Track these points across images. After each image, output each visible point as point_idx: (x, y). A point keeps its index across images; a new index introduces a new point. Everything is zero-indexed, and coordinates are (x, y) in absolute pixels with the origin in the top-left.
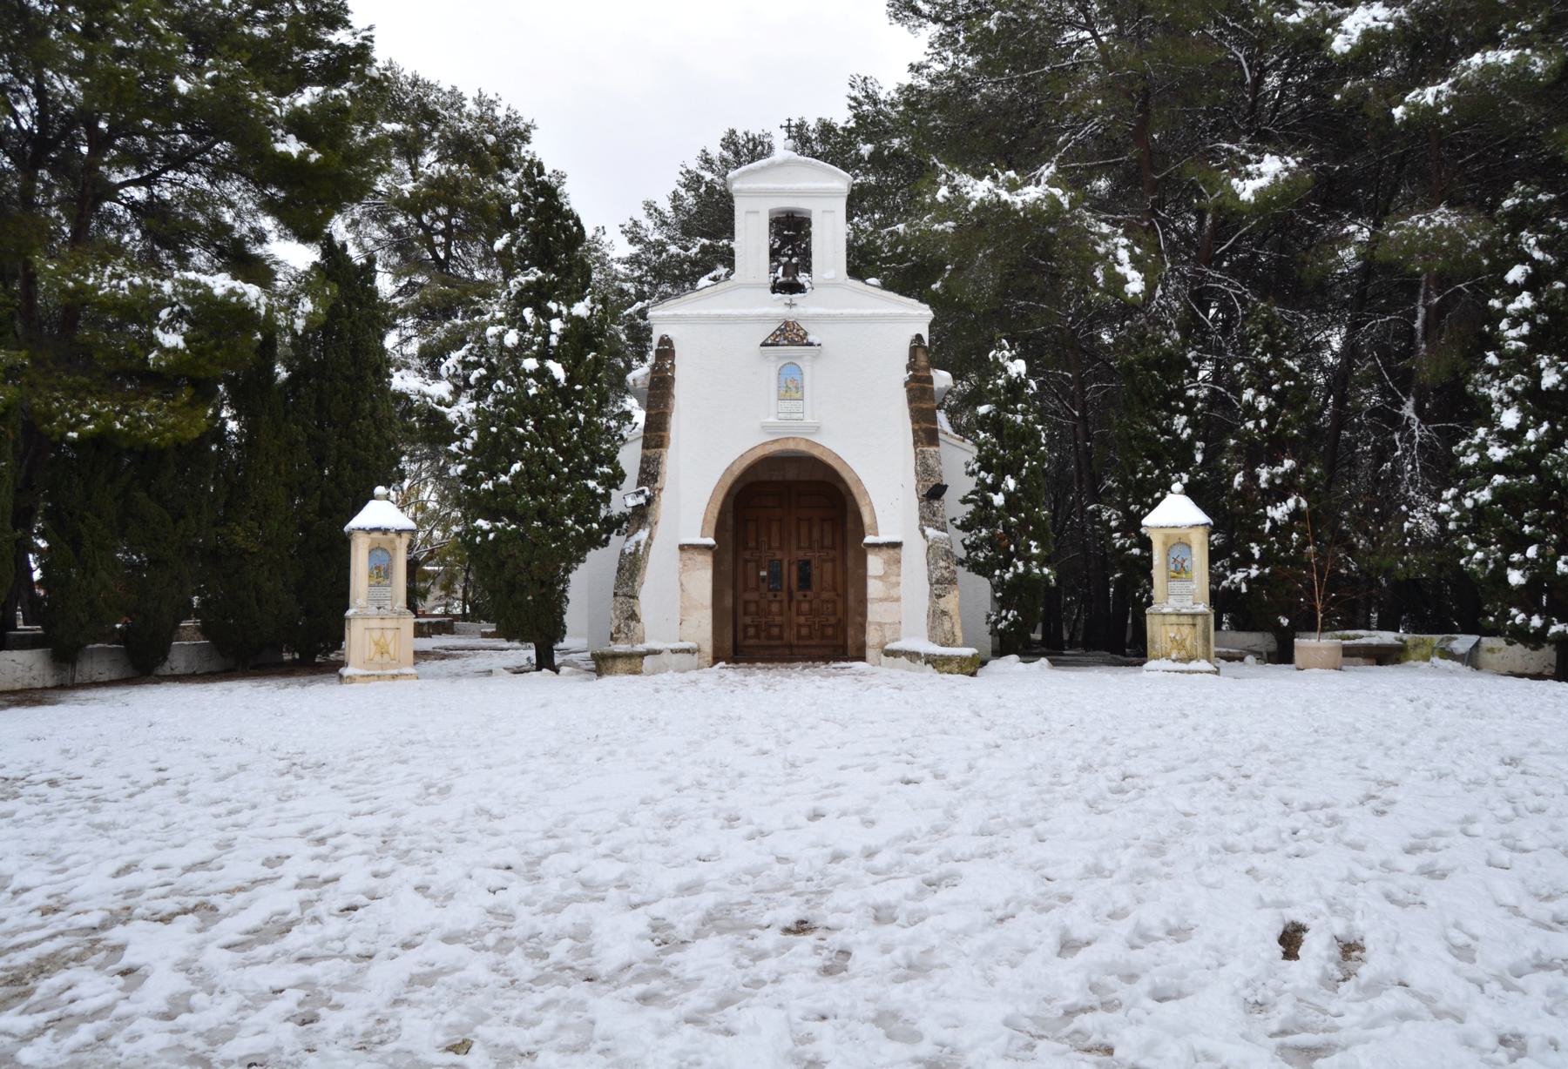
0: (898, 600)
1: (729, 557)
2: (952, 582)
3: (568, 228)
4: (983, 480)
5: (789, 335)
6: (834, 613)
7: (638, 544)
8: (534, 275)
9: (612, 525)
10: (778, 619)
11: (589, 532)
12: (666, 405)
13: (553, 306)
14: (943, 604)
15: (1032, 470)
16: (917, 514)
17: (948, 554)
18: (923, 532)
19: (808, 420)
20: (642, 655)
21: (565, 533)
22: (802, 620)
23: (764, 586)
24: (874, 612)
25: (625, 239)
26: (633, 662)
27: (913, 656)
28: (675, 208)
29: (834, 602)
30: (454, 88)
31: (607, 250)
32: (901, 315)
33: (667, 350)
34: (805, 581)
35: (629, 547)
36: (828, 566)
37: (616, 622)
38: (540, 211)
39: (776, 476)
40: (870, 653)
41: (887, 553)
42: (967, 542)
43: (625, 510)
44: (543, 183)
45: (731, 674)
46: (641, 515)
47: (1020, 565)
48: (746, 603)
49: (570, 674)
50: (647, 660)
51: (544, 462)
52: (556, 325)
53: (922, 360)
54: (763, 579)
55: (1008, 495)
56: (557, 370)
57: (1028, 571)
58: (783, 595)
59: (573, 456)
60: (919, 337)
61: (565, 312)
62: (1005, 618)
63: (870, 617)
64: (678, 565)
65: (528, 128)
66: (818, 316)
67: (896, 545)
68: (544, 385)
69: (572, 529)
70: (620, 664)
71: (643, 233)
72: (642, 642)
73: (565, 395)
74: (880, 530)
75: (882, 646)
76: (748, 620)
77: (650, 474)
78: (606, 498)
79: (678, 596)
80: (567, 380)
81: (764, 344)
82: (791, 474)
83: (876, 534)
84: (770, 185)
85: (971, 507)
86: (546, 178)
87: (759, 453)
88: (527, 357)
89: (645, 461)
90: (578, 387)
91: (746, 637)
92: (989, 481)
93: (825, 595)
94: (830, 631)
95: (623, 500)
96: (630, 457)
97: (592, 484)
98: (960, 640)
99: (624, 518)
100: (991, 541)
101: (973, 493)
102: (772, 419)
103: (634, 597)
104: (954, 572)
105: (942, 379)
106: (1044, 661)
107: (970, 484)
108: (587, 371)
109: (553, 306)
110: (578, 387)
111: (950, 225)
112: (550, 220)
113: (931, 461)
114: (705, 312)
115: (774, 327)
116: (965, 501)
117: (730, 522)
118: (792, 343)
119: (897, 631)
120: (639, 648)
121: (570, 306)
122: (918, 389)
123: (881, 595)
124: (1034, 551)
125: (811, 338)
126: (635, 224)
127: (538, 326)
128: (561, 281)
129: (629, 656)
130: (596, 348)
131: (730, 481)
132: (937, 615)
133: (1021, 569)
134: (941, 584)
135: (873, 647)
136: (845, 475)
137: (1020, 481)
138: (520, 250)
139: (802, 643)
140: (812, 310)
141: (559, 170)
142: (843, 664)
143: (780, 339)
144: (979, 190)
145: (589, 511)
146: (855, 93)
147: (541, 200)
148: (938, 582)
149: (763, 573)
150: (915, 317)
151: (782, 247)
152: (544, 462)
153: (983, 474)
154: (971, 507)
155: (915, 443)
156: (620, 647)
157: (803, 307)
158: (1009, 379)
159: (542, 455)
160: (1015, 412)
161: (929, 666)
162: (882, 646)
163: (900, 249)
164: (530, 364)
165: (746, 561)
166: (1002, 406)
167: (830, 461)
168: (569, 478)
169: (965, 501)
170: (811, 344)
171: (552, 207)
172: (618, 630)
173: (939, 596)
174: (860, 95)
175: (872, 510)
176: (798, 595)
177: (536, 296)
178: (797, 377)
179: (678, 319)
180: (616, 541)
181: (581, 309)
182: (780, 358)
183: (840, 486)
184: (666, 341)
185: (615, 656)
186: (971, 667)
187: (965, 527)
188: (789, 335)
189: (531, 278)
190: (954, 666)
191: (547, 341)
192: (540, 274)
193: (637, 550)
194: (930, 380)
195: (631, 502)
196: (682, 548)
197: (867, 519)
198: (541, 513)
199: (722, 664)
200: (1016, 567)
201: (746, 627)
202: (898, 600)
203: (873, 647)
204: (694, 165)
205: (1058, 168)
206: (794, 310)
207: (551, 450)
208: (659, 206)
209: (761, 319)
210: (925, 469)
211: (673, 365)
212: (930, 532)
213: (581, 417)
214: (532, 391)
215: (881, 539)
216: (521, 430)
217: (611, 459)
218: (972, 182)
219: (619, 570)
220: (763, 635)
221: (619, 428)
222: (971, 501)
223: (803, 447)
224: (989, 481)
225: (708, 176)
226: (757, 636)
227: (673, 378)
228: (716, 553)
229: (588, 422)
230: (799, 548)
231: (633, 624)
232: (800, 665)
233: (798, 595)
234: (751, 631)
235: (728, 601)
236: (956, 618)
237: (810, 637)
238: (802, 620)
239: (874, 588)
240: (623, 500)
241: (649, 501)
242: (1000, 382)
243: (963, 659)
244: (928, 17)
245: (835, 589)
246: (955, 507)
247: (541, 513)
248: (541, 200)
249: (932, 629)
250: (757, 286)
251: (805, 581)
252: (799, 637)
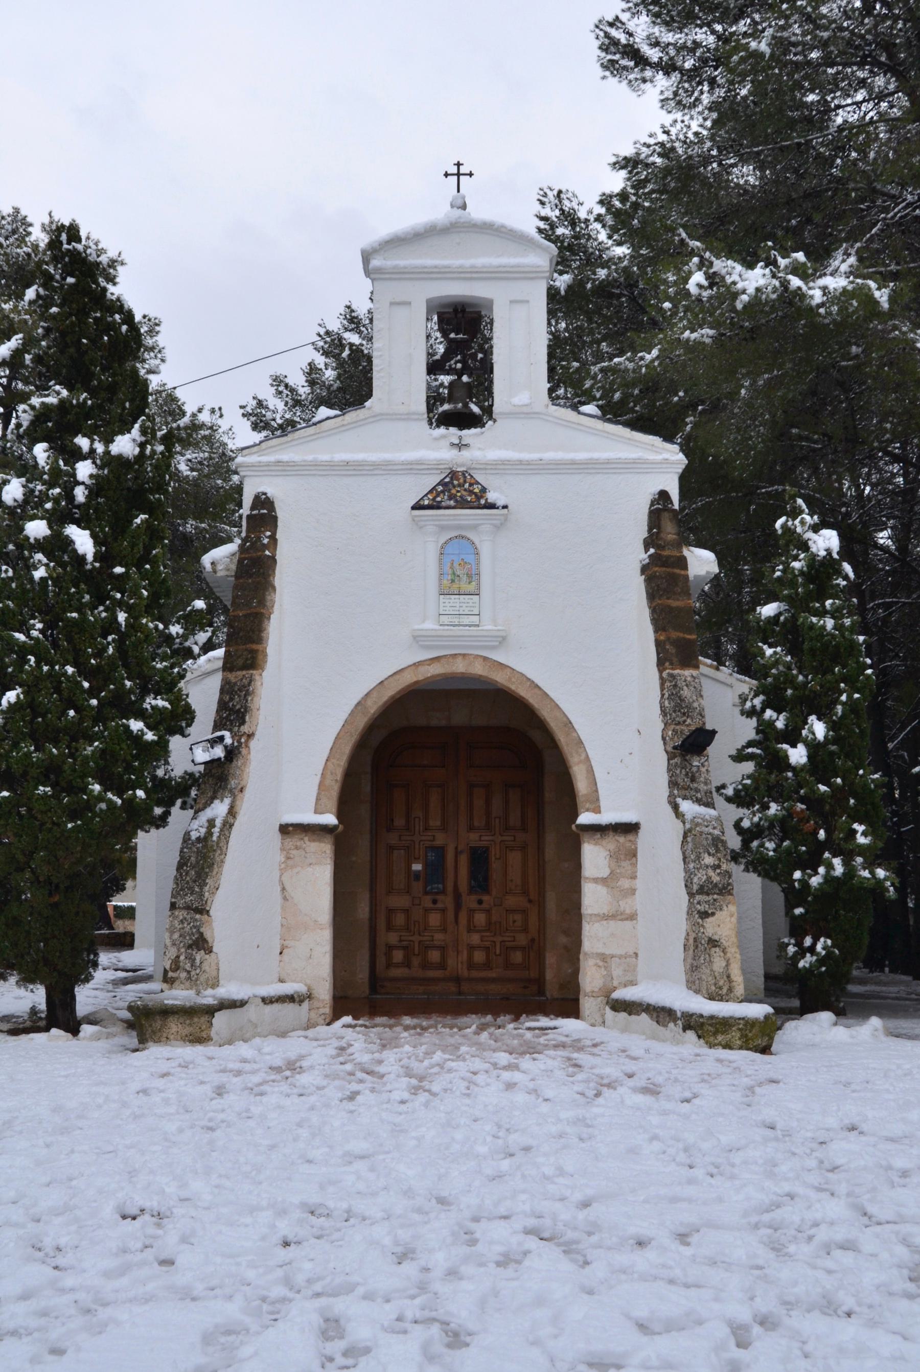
0: (632, 917)
1: (364, 843)
2: (725, 890)
3: (114, 327)
4: (771, 723)
5: (457, 492)
6: (525, 930)
7: (211, 823)
8: (57, 394)
9: (172, 792)
10: (439, 937)
11: (130, 803)
12: (262, 602)
13: (83, 442)
14: (711, 927)
15: (851, 706)
16: (663, 779)
17: (718, 843)
18: (676, 807)
19: (488, 626)
20: (210, 1011)
21: (89, 806)
22: (475, 939)
23: (417, 887)
24: (595, 937)
25: (247, 424)
26: (196, 1022)
27: (662, 1014)
28: (312, 383)
29: (524, 912)
30: (17, 211)
31: (225, 439)
32: (635, 462)
33: (265, 514)
34: (480, 877)
35: (198, 828)
36: (515, 858)
37: (173, 952)
38: (69, 297)
39: (437, 720)
40: (588, 1005)
41: (612, 842)
42: (746, 824)
43: (191, 768)
44: (74, 254)
45: (355, 1037)
46: (218, 777)
47: (837, 862)
48: (390, 911)
49: (96, 1037)
50: (220, 1019)
51: (58, 690)
52: (84, 470)
53: (670, 531)
54: (417, 875)
55: (814, 748)
56: (82, 541)
57: (850, 872)
58: (447, 901)
59: (108, 680)
60: (663, 495)
61: (100, 448)
62: (812, 950)
63: (588, 945)
64: (279, 857)
65: (113, 263)
66: (504, 462)
67: (631, 829)
68: (61, 564)
69: (101, 798)
70: (174, 1026)
71: (269, 415)
72: (215, 984)
73: (94, 581)
74: (603, 803)
75: (606, 993)
76: (393, 938)
77: (234, 711)
78: (160, 750)
79: (274, 907)
80: (97, 557)
81: (417, 507)
82: (460, 717)
83: (597, 810)
84: (429, 262)
85: (749, 767)
86: (80, 247)
87: (409, 679)
88: (33, 518)
89: (227, 689)
90: (119, 570)
91: (389, 965)
92: (780, 725)
93: (511, 901)
94: (518, 957)
95: (187, 754)
96: (202, 686)
97: (136, 725)
98: (740, 990)
99: (190, 780)
100: (784, 827)
101: (750, 744)
102: (430, 625)
103: (202, 910)
104: (728, 874)
105: (702, 562)
106: (875, 1022)
107: (748, 729)
108: (133, 546)
109: (83, 442)
110: (119, 570)
111: (706, 333)
112: (83, 313)
113: (686, 692)
114: (325, 457)
115: (432, 480)
116: (740, 757)
117: (366, 788)
118: (462, 504)
119: (633, 969)
120: (208, 997)
121: (108, 440)
122: (662, 575)
123: (605, 910)
124: (861, 840)
125: (491, 496)
126: (260, 404)
127: (55, 472)
128: (100, 407)
129: (189, 1012)
130: (150, 509)
131: (361, 722)
132: (701, 947)
133: (839, 868)
134: (706, 895)
135: (593, 995)
136: (546, 713)
137: (832, 726)
138: (38, 360)
139: (475, 974)
140: (494, 454)
141: (152, 315)
142: (544, 1022)
143: (443, 499)
144: (752, 280)
145: (129, 769)
146: (546, 211)
147: (70, 280)
148: (702, 890)
149: (417, 867)
150: (660, 464)
151: (447, 356)
152: (58, 690)
153: (769, 714)
154: (749, 767)
155: (661, 664)
156: (179, 996)
157: (482, 448)
158: (812, 559)
159: (56, 679)
160: (822, 613)
161: (691, 1035)
162: (606, 993)
163: (617, 395)
164: (37, 529)
165: (391, 848)
166: (798, 604)
167: (523, 692)
168: (100, 716)
169: (740, 757)
170: (492, 506)
171: (89, 292)
172: (176, 965)
173: (705, 915)
174: (554, 214)
175: (590, 771)
176: (470, 901)
177: (57, 427)
178: (470, 558)
179: (283, 468)
180: (178, 816)
181: (125, 445)
182: (443, 528)
183: (536, 736)
184: (263, 502)
185: (167, 1012)
186: (759, 1038)
187: (741, 799)
188: (457, 492)
189: (52, 400)
190: (735, 1035)
191: (69, 496)
192: (65, 393)
193: (209, 833)
194: (682, 563)
195: (202, 755)
196: (286, 830)
197: (581, 786)
198: (50, 772)
199: (347, 1019)
200: (830, 867)
201: (390, 948)
202: (632, 917)
203: (593, 995)
204: (335, 325)
205: (860, 260)
206: (465, 453)
207: (70, 670)
208: (291, 381)
209: (412, 468)
210: (676, 706)
211: (273, 539)
212: (687, 807)
213: (122, 617)
214: (40, 574)
215: (606, 817)
216: (21, 637)
217: (168, 685)
218: (739, 268)
219: (180, 866)
220: (416, 961)
221: (185, 637)
222: (751, 757)
223: (478, 669)
224: (780, 725)
225: (353, 338)
226: (407, 964)
227: (273, 559)
228: (341, 839)
229: (133, 625)
230: (471, 828)
231: (199, 956)
232: (473, 1022)
233: (470, 901)
234: (398, 956)
235: (363, 910)
236: (733, 951)
237: (487, 965)
238: (475, 939)
239: (593, 898)
240: (187, 754)
241: (232, 753)
242: (796, 565)
243: (749, 1023)
244: (659, 66)
245: (525, 892)
246: (724, 768)
247: (50, 772)
248: (70, 280)
249: (693, 969)
250: (408, 417)
251: (480, 877)
252: (471, 965)
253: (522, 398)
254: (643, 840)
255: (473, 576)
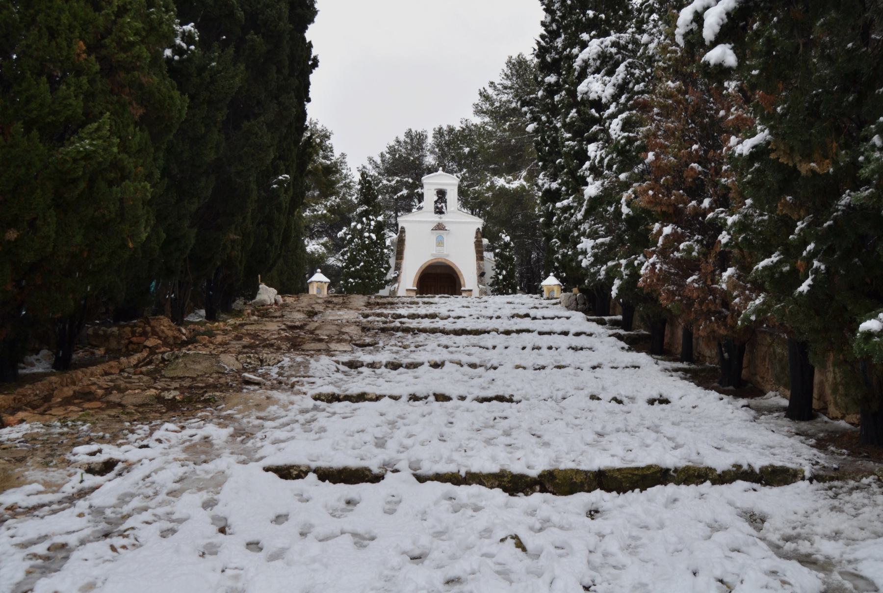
5: (440, 227)
8: (365, 207)
9: (387, 282)
13: (371, 217)
35: (392, 289)
46: (395, 280)
52: (373, 223)
53: (480, 235)
67: (471, 291)
77: (398, 268)
109: (371, 217)
126: (364, 167)
140: (447, 220)
157: (444, 219)
159: (369, 261)
166: (503, 250)
179: (406, 221)
184: (403, 228)
187: (491, 285)
188: (440, 227)
195: (393, 276)
198: (368, 278)
209: (432, 222)
217: (387, 262)
240: (391, 275)
253: (452, 209)
254: (473, 293)
255: (443, 243)
